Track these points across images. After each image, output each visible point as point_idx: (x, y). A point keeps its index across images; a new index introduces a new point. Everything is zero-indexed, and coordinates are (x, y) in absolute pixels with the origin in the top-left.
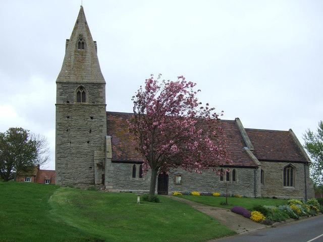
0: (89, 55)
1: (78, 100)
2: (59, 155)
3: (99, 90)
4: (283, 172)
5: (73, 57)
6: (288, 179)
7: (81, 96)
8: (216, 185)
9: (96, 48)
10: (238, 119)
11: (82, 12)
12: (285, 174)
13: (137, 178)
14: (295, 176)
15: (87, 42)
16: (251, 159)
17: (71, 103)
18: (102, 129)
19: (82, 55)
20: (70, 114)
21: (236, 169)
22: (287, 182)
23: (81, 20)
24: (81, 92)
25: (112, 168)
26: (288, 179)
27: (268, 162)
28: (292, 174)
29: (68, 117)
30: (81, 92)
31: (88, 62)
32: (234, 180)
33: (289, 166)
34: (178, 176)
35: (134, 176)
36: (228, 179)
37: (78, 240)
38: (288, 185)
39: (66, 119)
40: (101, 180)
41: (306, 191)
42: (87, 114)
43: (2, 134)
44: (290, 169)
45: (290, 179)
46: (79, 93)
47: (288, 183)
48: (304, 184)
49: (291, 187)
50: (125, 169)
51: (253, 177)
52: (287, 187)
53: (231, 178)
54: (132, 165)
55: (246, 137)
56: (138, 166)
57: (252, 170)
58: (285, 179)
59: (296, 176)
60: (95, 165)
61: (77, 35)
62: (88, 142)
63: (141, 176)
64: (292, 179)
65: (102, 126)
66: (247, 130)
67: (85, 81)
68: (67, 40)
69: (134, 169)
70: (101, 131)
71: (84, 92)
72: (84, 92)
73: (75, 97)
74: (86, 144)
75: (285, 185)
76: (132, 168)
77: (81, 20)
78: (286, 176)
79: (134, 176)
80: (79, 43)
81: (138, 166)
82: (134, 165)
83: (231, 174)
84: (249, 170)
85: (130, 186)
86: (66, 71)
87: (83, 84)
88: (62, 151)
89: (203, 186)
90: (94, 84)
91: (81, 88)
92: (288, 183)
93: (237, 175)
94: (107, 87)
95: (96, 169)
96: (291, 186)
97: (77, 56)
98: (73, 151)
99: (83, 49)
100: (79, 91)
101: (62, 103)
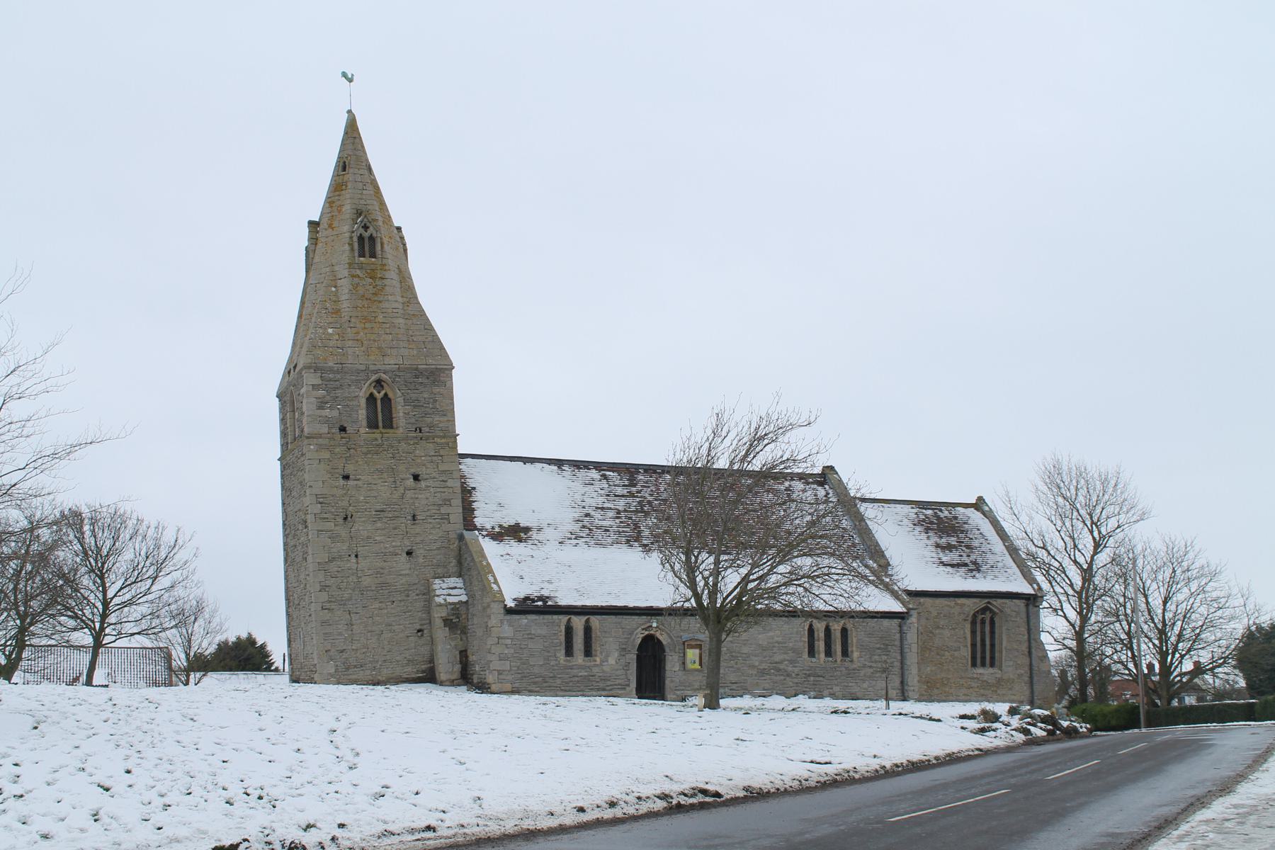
0: (392, 274)
1: (372, 425)
3: (436, 390)
4: (968, 626)
5: (345, 285)
6: (983, 645)
8: (796, 670)
9: (405, 250)
10: (832, 468)
11: (352, 132)
12: (973, 632)
13: (579, 658)
14: (1001, 636)
15: (383, 234)
18: (449, 510)
20: (350, 469)
21: (595, 621)
22: (979, 655)
23: (352, 162)
24: (379, 396)
25: (507, 631)
26: (983, 645)
28: (992, 632)
29: (346, 477)
30: (379, 396)
31: (394, 300)
32: (845, 653)
33: (984, 610)
34: (692, 647)
35: (569, 652)
36: (828, 653)
37: (696, 847)
38: (983, 665)
39: (342, 482)
40: (458, 667)
41: (1031, 677)
42: (402, 468)
44: (988, 616)
45: (988, 647)
46: (371, 399)
47: (983, 658)
48: (1027, 661)
49: (991, 670)
50: (542, 631)
51: (897, 643)
52: (980, 670)
53: (838, 647)
54: (564, 619)
58: (974, 645)
59: (1004, 638)
60: (438, 623)
61: (348, 209)
62: (409, 553)
63: (588, 652)
64: (992, 646)
65: (447, 502)
67: (391, 361)
68: (311, 223)
69: (569, 631)
70: (446, 518)
71: (386, 395)
72: (386, 395)
73: (362, 414)
75: (974, 665)
76: (563, 628)
77: (352, 162)
78: (978, 639)
79: (569, 652)
80: (361, 238)
82: (587, 621)
83: (820, 633)
84: (886, 622)
85: (559, 681)
86: (330, 331)
88: (331, 582)
89: (763, 672)
90: (417, 373)
91: (379, 383)
92: (983, 658)
93: (853, 639)
95: (441, 633)
96: (992, 665)
97: (356, 280)
98: (366, 581)
99: (373, 255)
100: (371, 394)
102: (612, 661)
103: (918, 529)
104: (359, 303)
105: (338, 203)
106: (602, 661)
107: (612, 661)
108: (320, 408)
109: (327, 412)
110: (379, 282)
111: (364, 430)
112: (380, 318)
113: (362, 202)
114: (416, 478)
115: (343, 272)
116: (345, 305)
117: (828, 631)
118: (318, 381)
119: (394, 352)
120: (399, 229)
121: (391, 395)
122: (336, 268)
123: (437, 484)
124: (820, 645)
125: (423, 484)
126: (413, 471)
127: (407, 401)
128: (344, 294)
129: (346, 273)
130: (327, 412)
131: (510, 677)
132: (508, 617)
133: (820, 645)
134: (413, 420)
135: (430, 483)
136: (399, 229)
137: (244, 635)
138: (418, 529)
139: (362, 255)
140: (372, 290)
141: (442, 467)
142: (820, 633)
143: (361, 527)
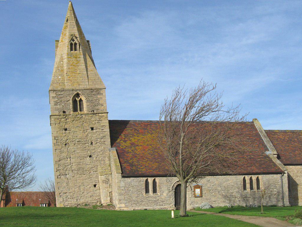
1: (75, 110)
2: (58, 173)
3: (99, 96)
5: (65, 61)
7: (77, 105)
16: (275, 165)
17: (67, 113)
19: (76, 58)
21: (260, 177)
27: (293, 166)
35: (147, 191)
36: (252, 188)
43: (5, 156)
54: (145, 179)
55: (266, 140)
56: (150, 180)
57: (279, 175)
62: (90, 156)
63: (155, 191)
66: (270, 133)
67: (81, 87)
71: (81, 99)
74: (88, 158)
79: (147, 191)
80: (71, 44)
81: (150, 180)
82: (154, 180)
83: (248, 181)
86: (60, 77)
87: (80, 90)
94: (299, 188)
101: (57, 113)
102: (165, 194)
103: (26, 156)
104: (70, 67)
105: (64, 33)
106: (161, 195)
107: (165, 194)
108: (55, 105)
109: (58, 106)
110: (78, 59)
111: (72, 112)
112: (78, 72)
113: (73, 32)
114: (92, 129)
115: (65, 56)
116: (65, 68)
117: (251, 179)
118: (55, 95)
119: (83, 83)
120: (88, 41)
121: (82, 99)
122: (63, 55)
123: (100, 131)
124: (248, 186)
125: (94, 131)
126: (90, 126)
127: (87, 101)
128: (65, 66)
129: (66, 57)
130: (58, 106)
131: (124, 202)
132: (123, 179)
133: (248, 186)
134: (91, 108)
135: (98, 130)
136: (88, 41)
137: (249, 119)
138: (92, 148)
139: (71, 50)
140: (75, 62)
141: (102, 125)
142: (248, 181)
143: (71, 147)
